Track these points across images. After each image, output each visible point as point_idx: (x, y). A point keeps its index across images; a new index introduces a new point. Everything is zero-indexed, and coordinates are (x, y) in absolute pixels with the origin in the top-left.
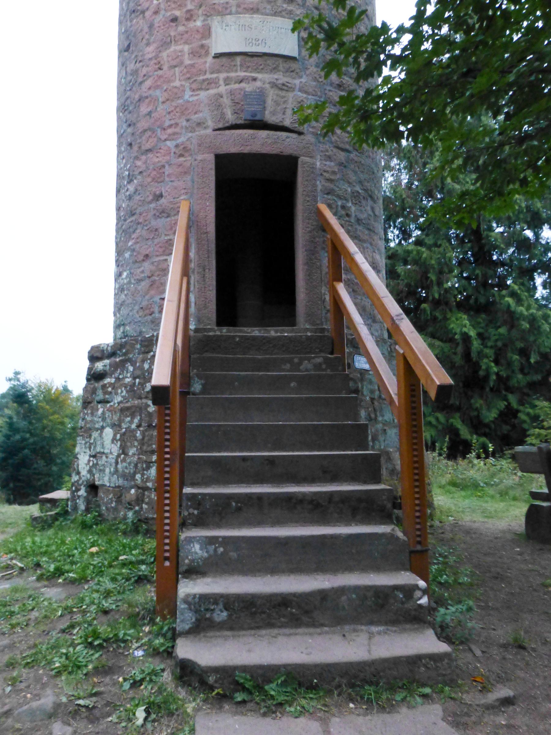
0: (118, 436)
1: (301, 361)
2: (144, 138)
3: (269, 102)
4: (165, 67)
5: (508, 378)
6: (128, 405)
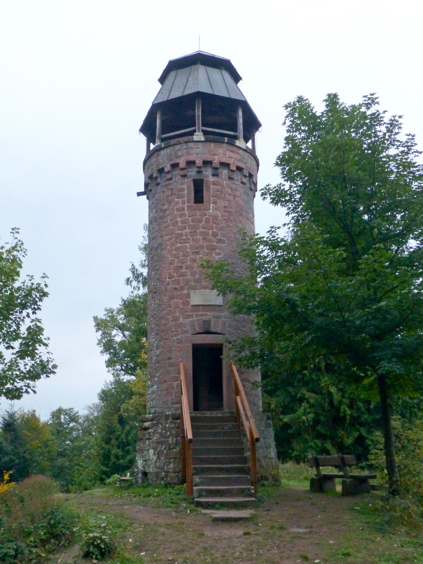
4: (172, 307)
5: (359, 417)
6: (161, 440)
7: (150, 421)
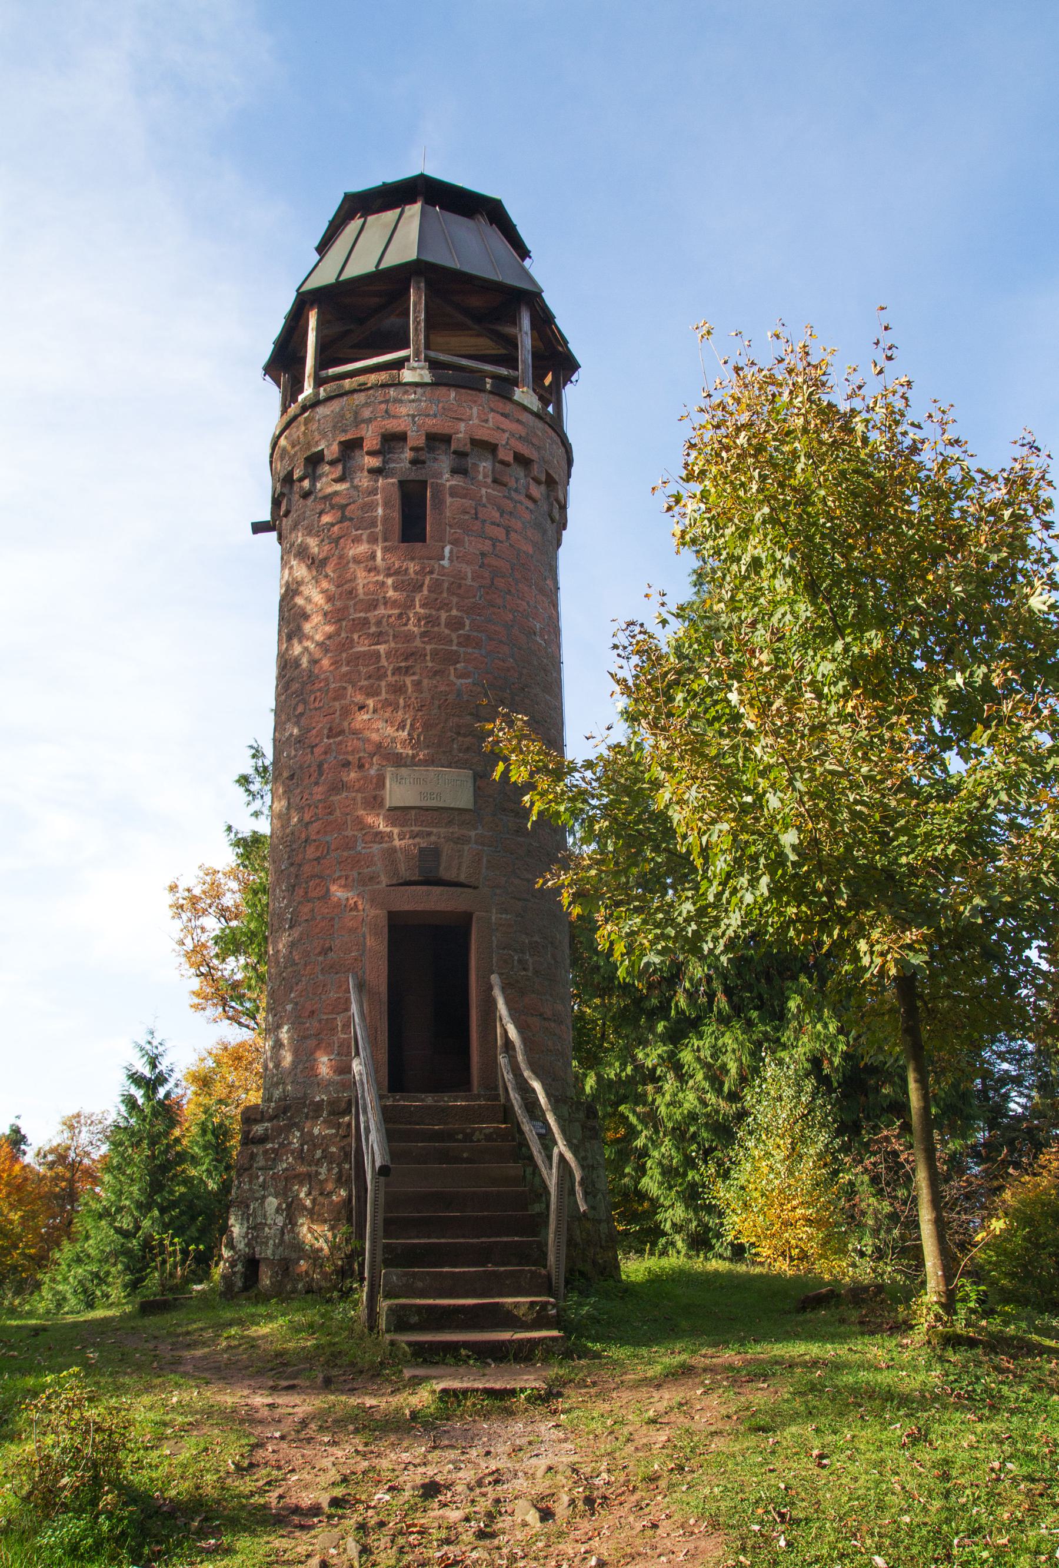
0: (284, 1206)
2: (311, 884)
3: (444, 858)
4: (338, 813)
7: (271, 1119)
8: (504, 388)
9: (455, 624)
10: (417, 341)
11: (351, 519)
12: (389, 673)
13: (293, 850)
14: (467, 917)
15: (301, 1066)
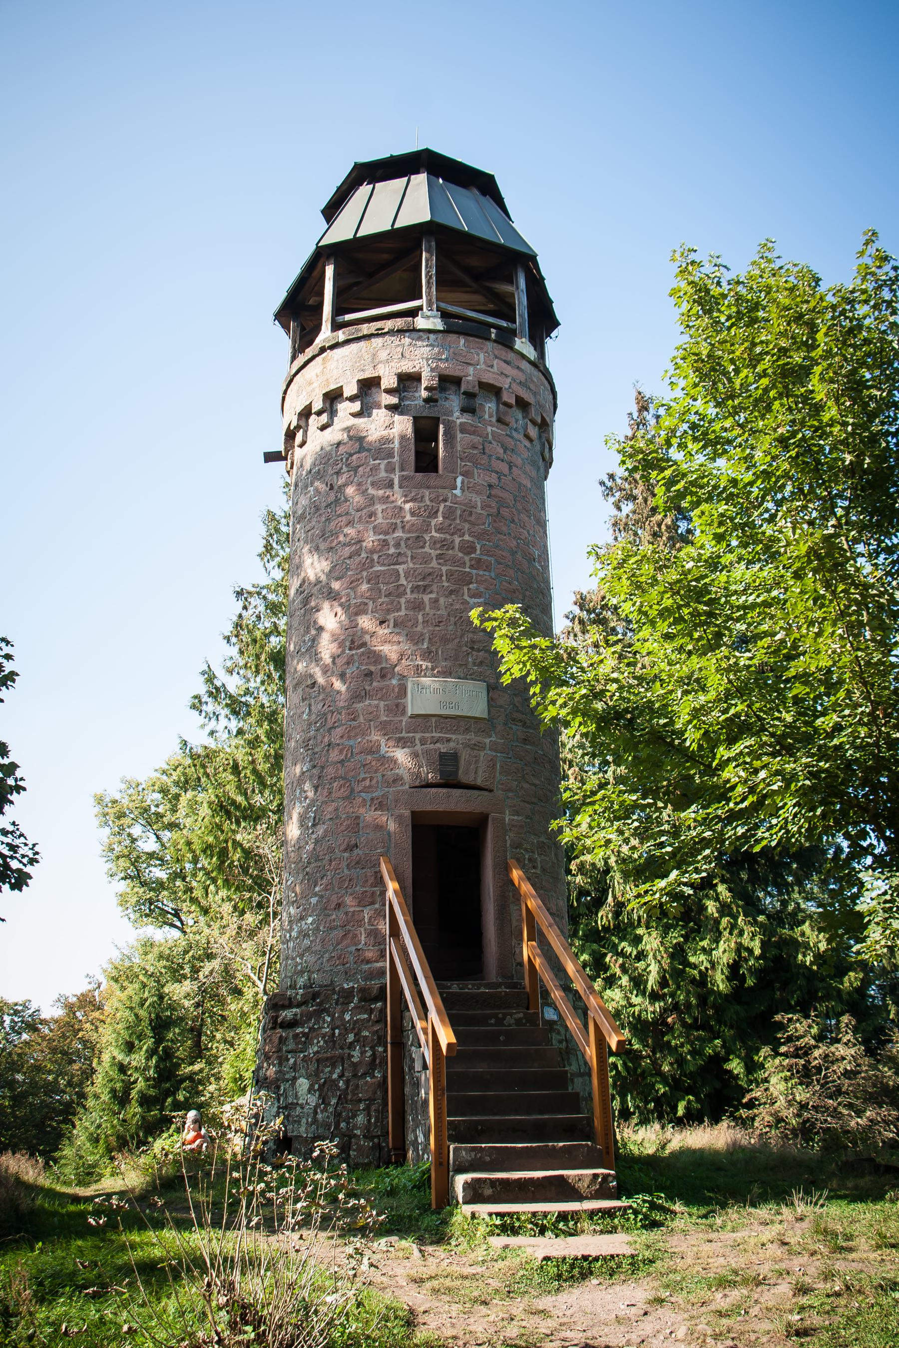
0: (316, 1087)
1: (505, 1015)
3: (462, 763)
4: (361, 719)
6: (329, 1055)
7: (299, 1005)
8: (506, 339)
9: (468, 549)
10: (429, 294)
11: (369, 450)
12: (408, 591)
13: (315, 754)
14: (483, 819)
15: (327, 955)
